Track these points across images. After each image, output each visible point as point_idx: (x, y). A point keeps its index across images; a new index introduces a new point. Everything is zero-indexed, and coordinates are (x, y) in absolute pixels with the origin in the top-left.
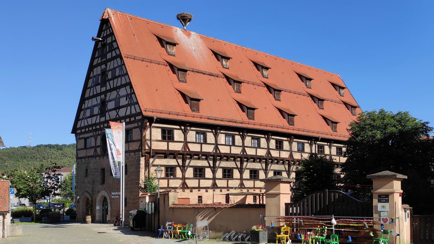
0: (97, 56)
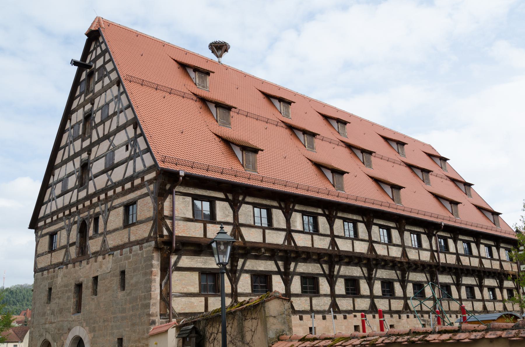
0: (78, 93)
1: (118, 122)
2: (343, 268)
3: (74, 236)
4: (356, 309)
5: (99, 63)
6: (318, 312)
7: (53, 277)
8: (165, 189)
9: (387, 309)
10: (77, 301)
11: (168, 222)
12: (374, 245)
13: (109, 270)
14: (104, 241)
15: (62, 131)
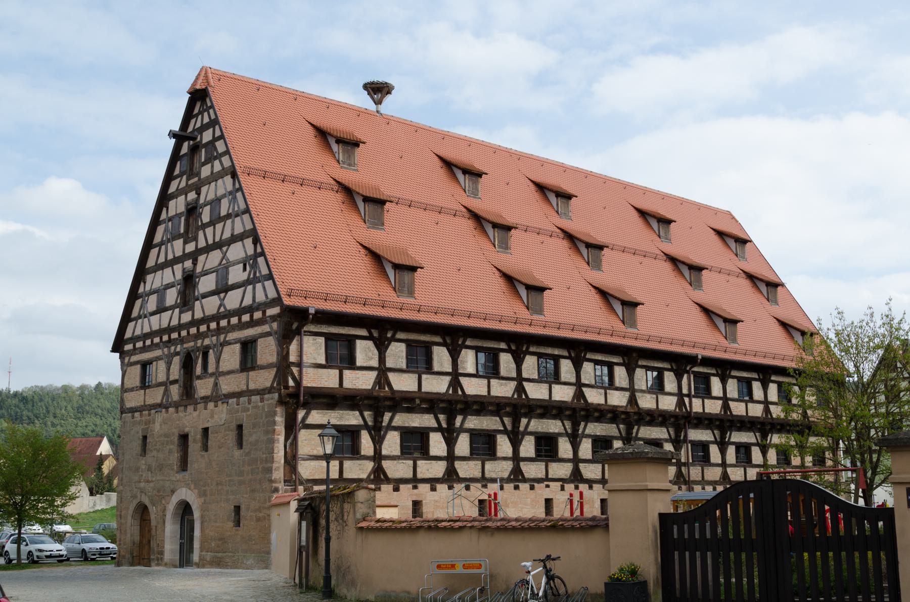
0: (177, 172)
1: (233, 229)
2: (533, 422)
3: (176, 371)
4: (550, 476)
5: (207, 136)
6: (493, 480)
7: (148, 423)
8: (291, 330)
9: (599, 476)
10: (181, 456)
11: (295, 370)
12: (584, 389)
13: (223, 421)
14: (216, 384)
15: (155, 222)
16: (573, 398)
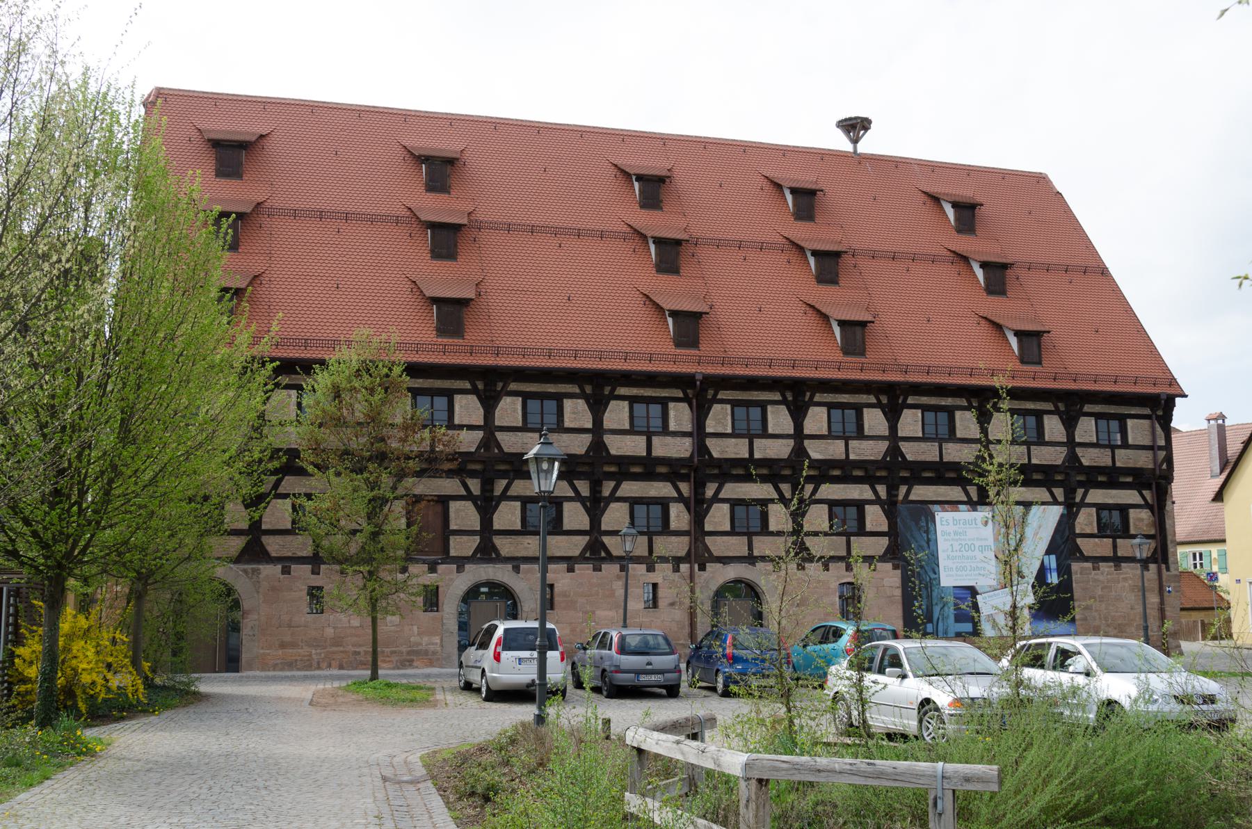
16: (479, 448)
